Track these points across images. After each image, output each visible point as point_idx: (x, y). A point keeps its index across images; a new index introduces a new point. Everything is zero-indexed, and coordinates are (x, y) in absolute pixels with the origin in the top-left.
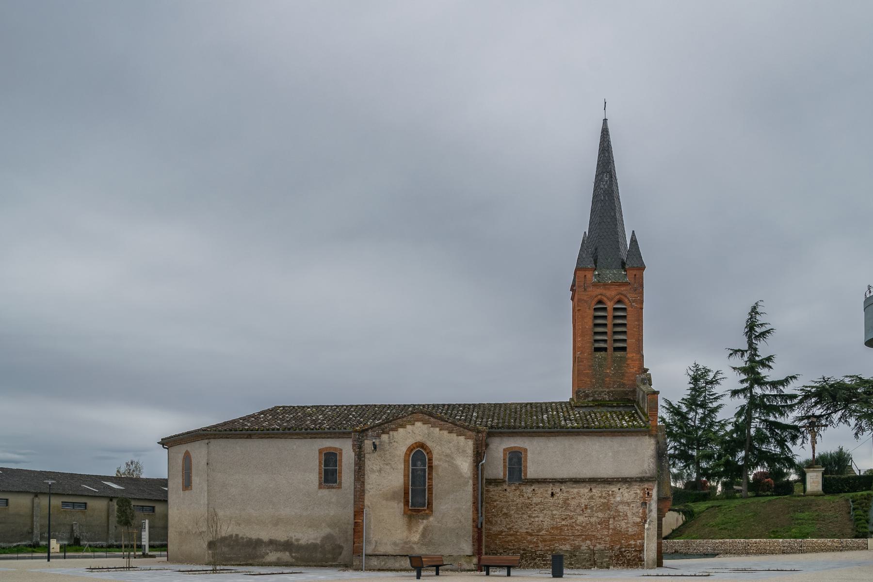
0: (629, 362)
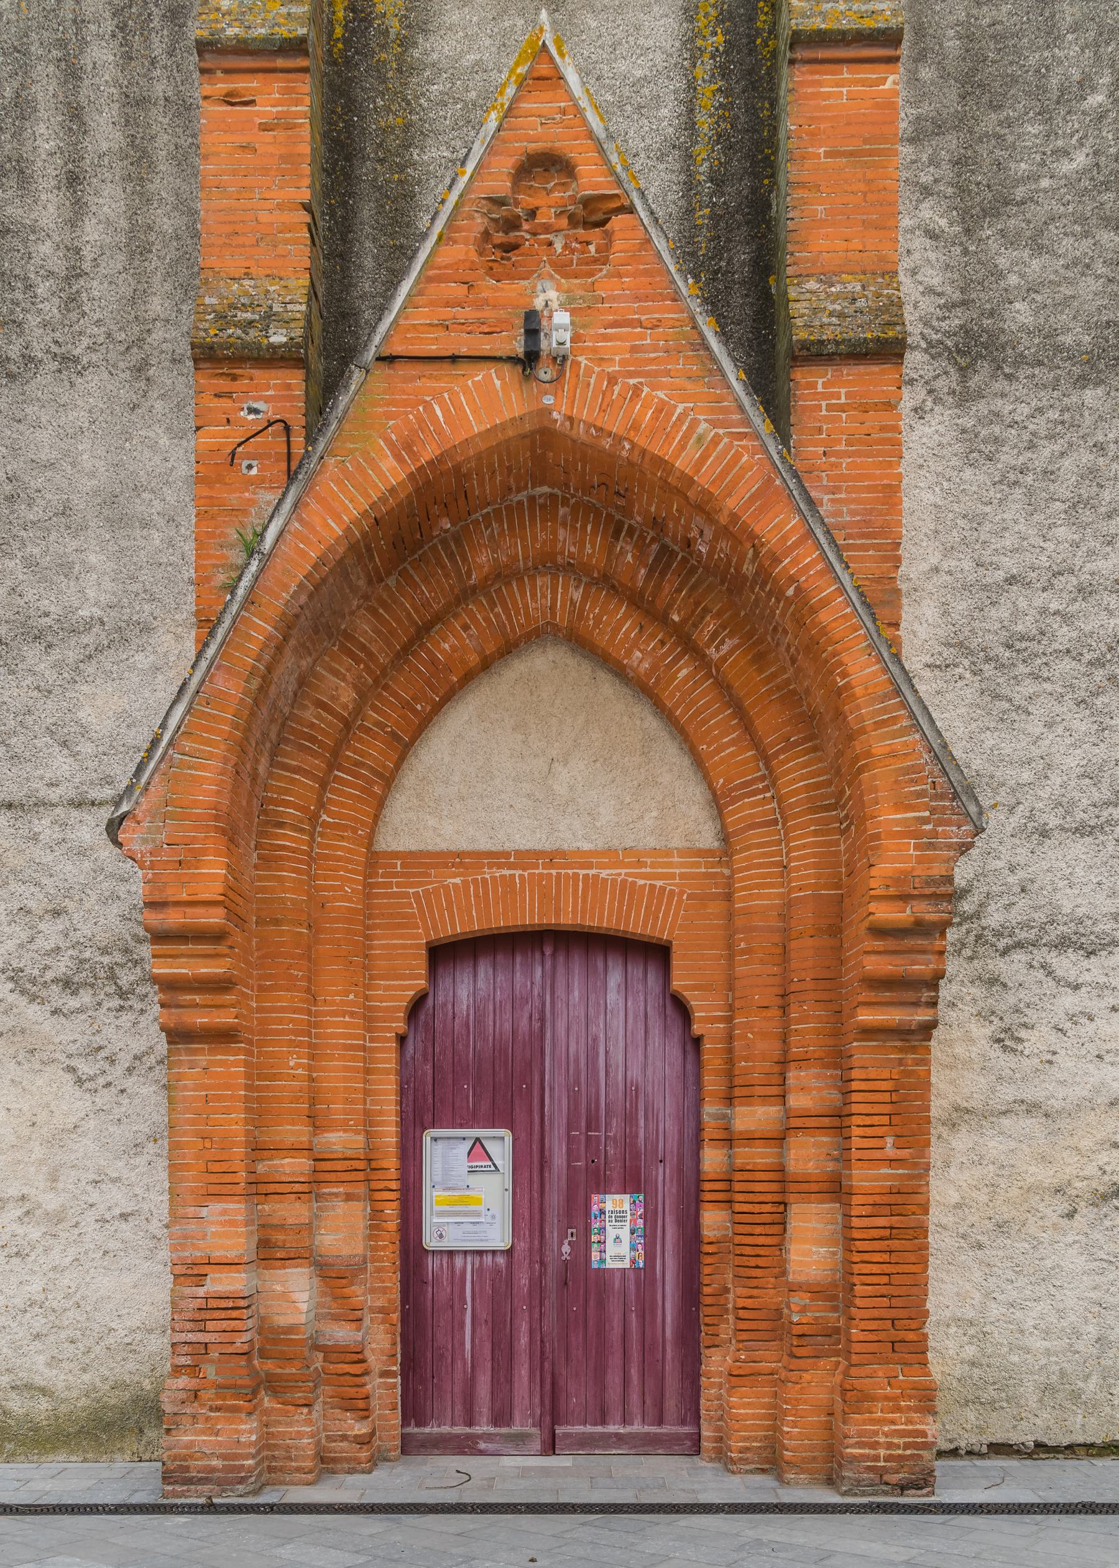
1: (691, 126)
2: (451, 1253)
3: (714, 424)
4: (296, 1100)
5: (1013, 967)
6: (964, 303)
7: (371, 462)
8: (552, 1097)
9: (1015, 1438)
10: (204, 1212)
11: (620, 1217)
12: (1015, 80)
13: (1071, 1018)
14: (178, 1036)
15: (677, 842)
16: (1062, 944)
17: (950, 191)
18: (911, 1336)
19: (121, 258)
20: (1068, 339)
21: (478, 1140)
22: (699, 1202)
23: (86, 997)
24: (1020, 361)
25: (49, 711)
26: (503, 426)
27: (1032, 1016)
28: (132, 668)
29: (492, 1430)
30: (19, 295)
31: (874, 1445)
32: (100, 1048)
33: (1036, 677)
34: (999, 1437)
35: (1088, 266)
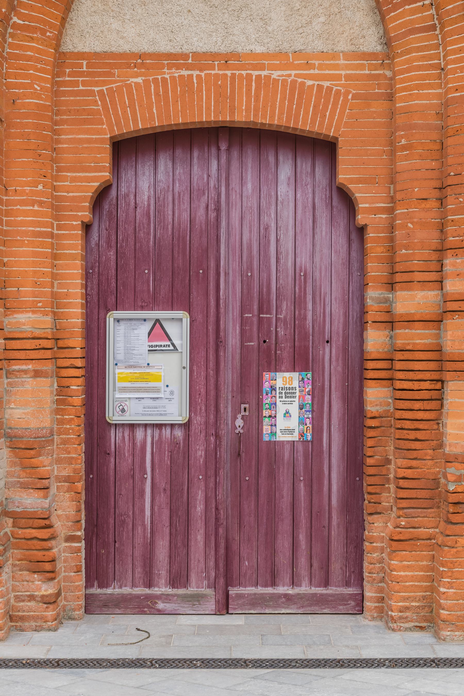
8: (226, 282)
21: (158, 321)
22: (362, 379)
29: (170, 591)
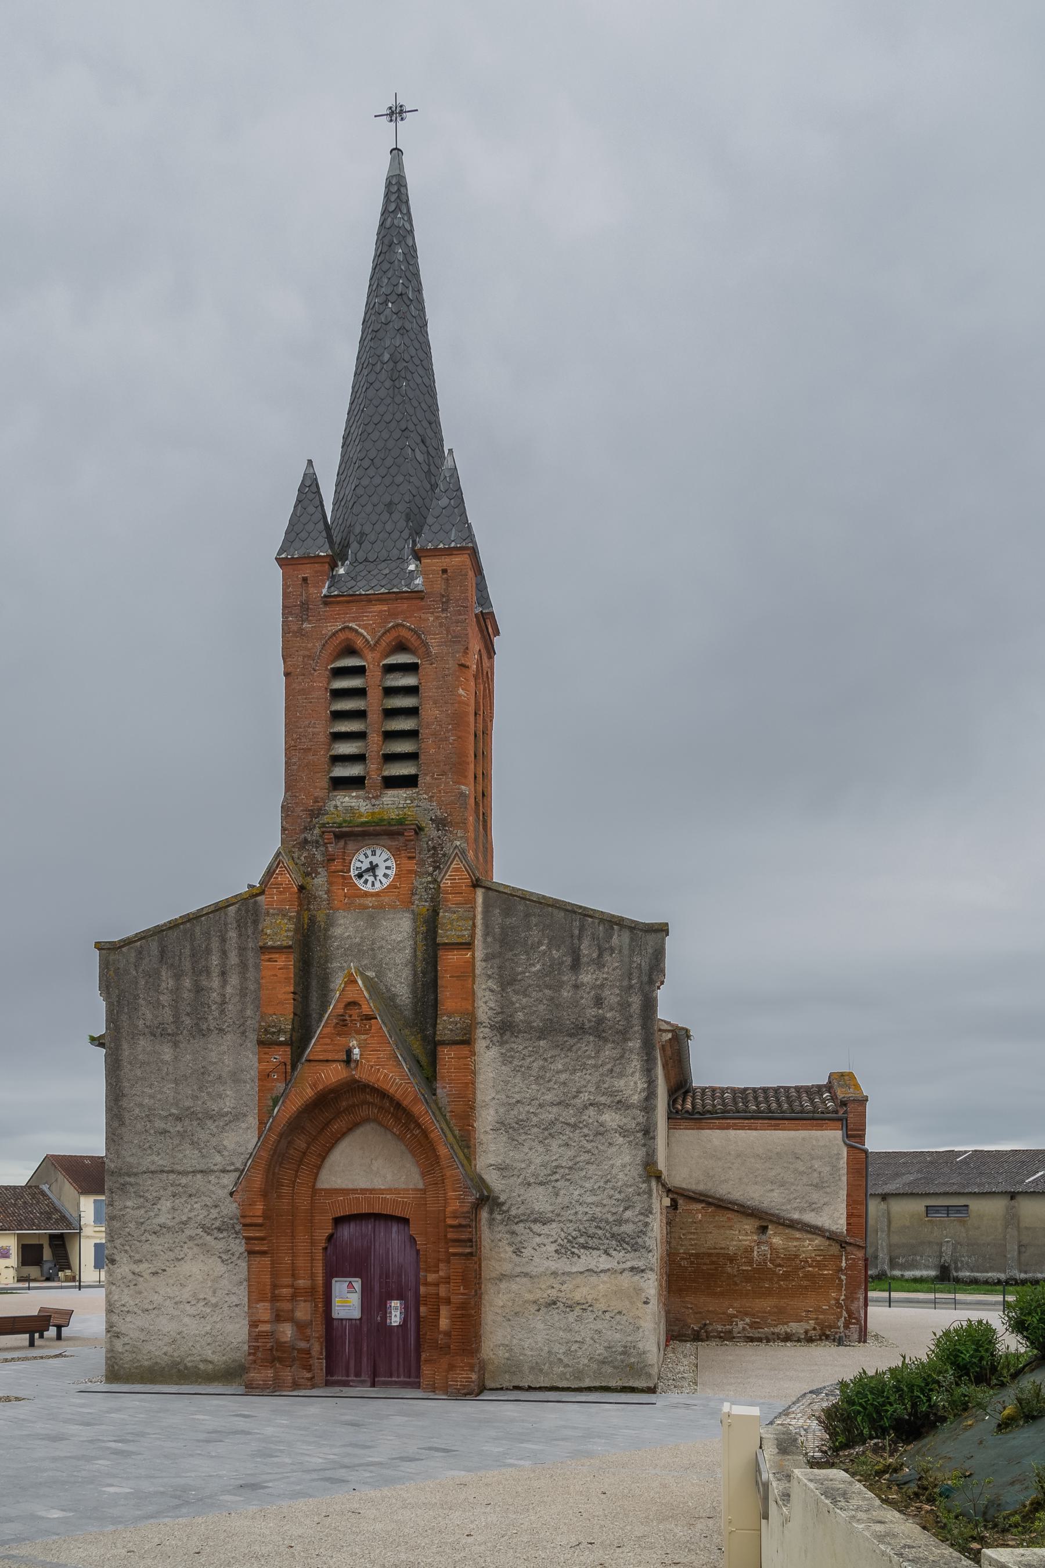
0: (323, 1134)
1: (415, 956)
2: (342, 1319)
3: (401, 1079)
4: (287, 1270)
5: (520, 1228)
6: (502, 1013)
7: (304, 1090)
8: (374, 1268)
9: (521, 1385)
10: (258, 1306)
11: (396, 1308)
12: (517, 942)
13: (538, 1245)
14: (250, 1253)
15: (411, 1187)
16: (535, 1221)
17: (497, 977)
18: (468, 1348)
19: (238, 997)
20: (535, 1024)
21: (350, 1282)
22: (419, 1304)
23: (225, 1234)
24: (520, 1031)
25: (214, 1141)
26: (341, 1079)
27: (526, 1244)
28: (240, 1128)
29: (355, 1378)
30: (206, 1009)
31: (457, 1381)
32: (229, 1251)
33: (526, 1133)
34: (516, 1384)
35: (541, 1001)
